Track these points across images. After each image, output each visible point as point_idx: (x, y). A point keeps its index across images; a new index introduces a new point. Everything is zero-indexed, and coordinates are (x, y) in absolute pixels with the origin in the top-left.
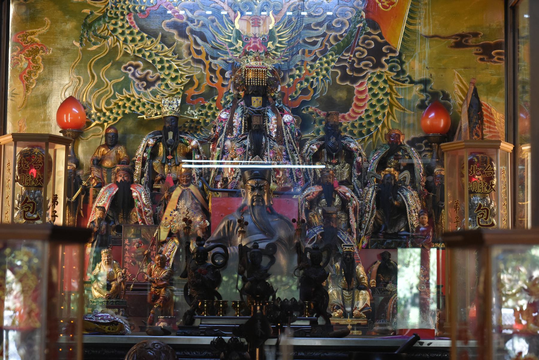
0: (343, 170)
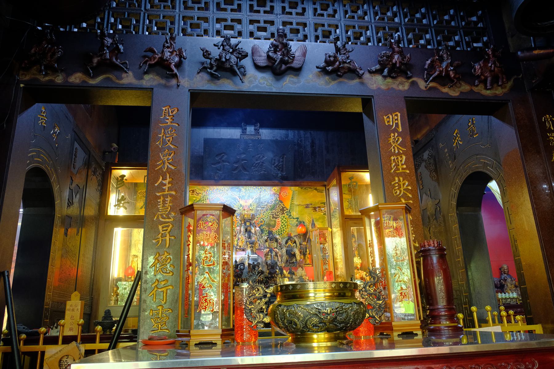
0: (275, 245)
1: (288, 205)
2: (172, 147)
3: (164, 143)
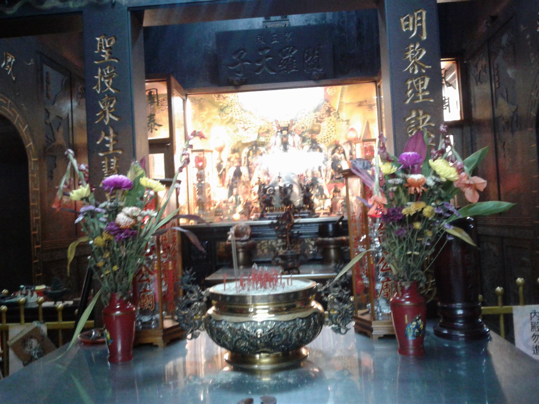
1: (336, 105)
2: (113, 91)
3: (103, 86)
